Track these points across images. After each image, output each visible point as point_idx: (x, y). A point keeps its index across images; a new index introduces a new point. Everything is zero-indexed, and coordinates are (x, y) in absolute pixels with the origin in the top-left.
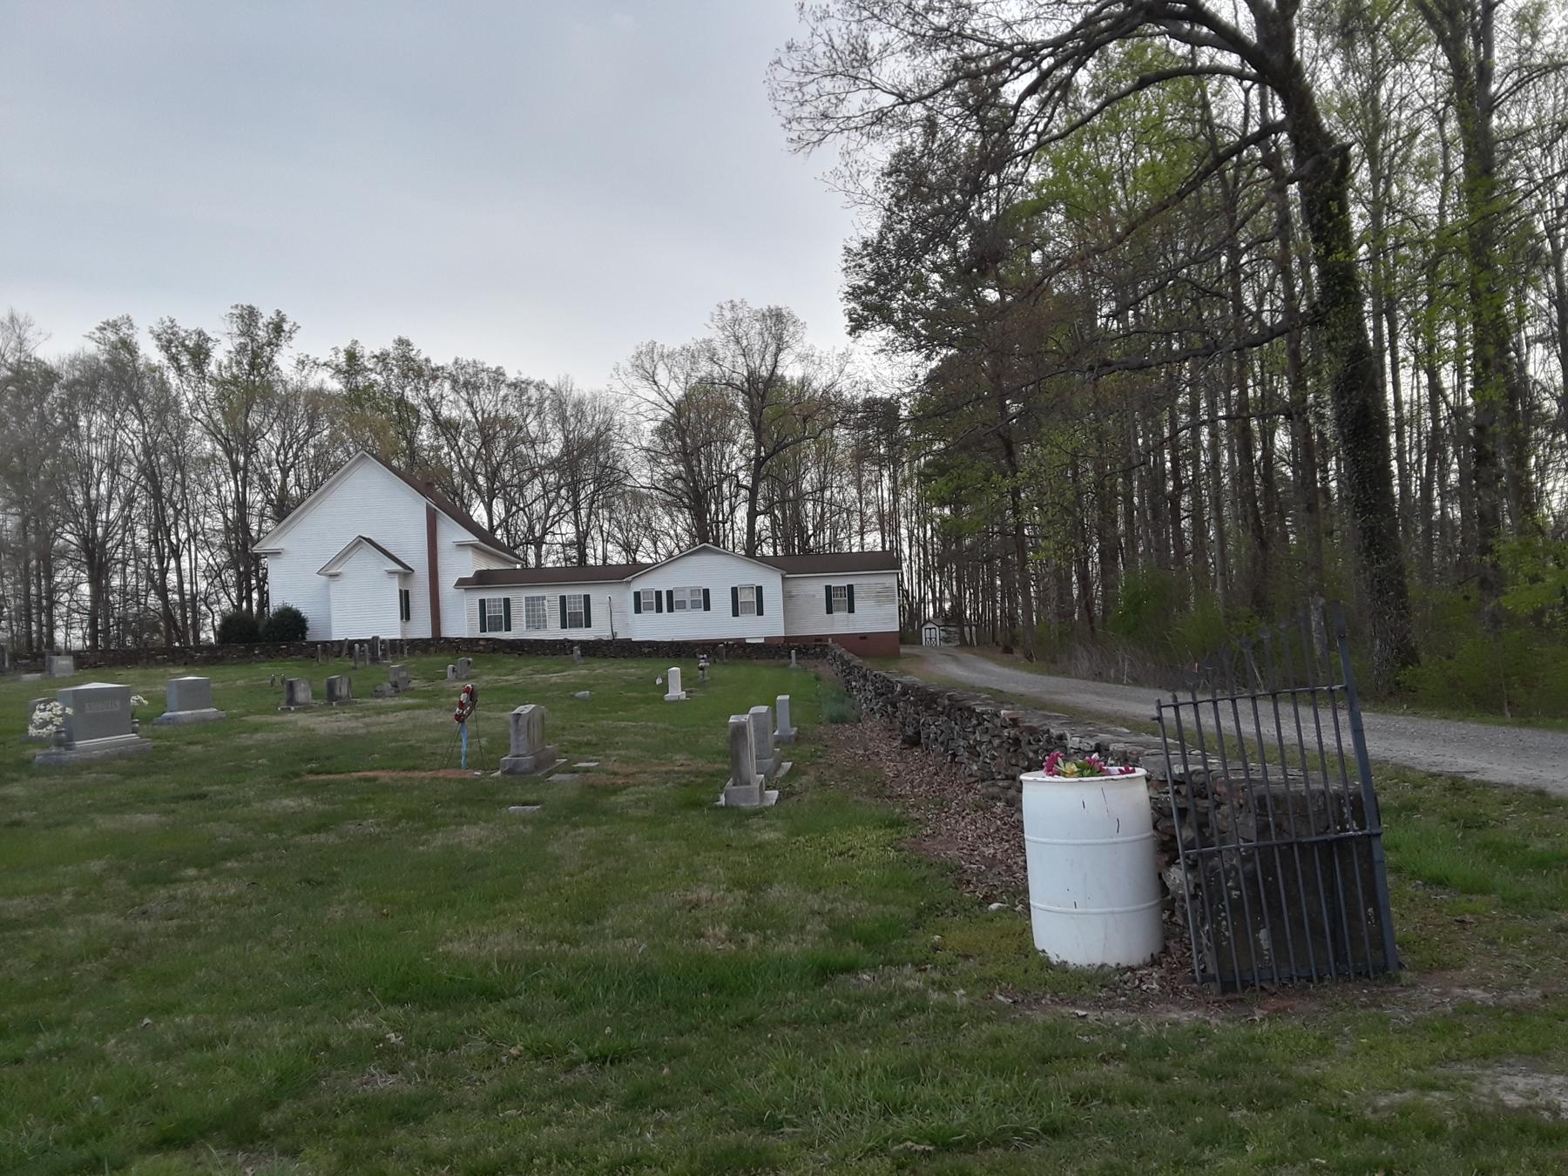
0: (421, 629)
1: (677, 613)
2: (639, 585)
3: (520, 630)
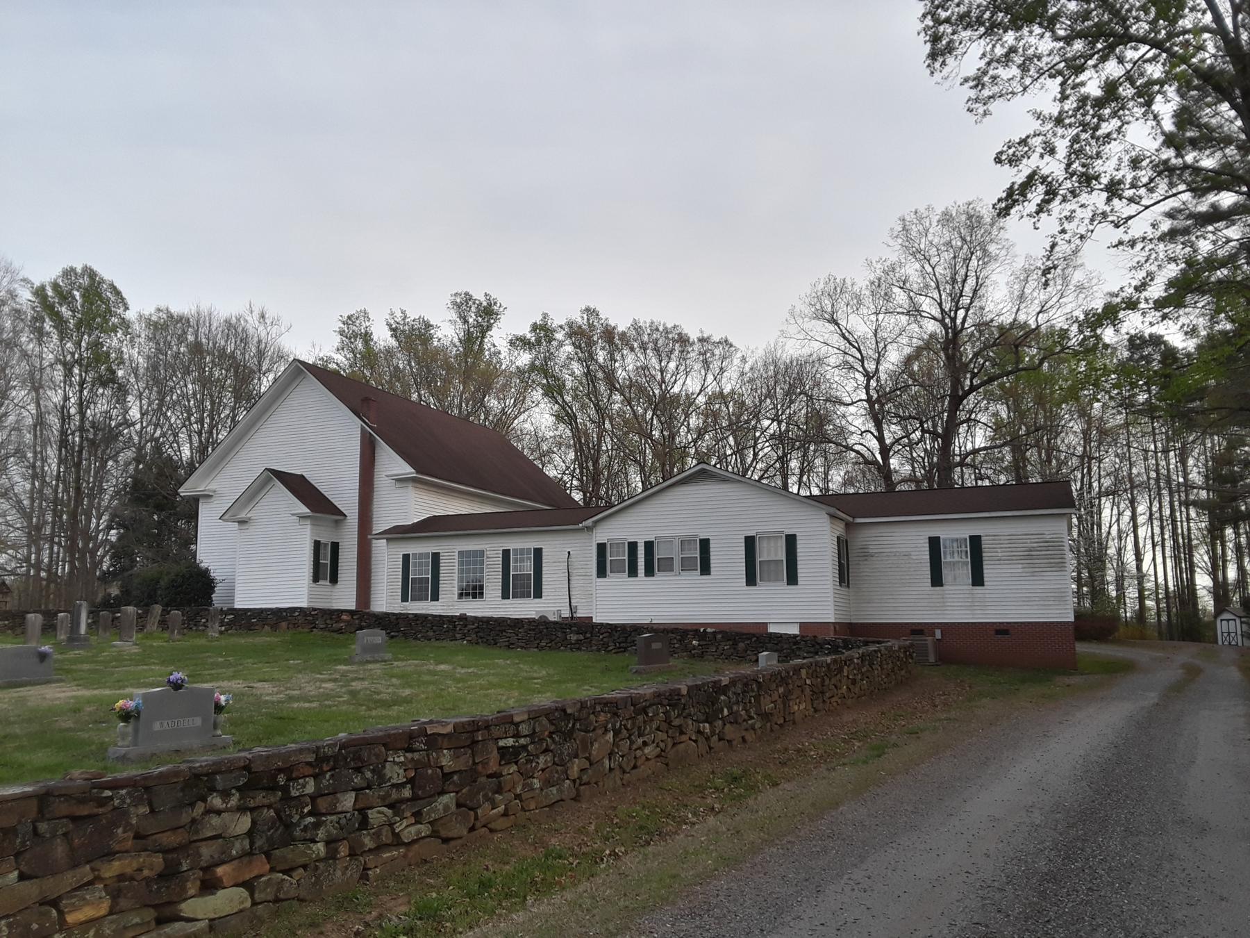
0: (344, 597)
1: (659, 577)
2: (604, 534)
3: (449, 604)
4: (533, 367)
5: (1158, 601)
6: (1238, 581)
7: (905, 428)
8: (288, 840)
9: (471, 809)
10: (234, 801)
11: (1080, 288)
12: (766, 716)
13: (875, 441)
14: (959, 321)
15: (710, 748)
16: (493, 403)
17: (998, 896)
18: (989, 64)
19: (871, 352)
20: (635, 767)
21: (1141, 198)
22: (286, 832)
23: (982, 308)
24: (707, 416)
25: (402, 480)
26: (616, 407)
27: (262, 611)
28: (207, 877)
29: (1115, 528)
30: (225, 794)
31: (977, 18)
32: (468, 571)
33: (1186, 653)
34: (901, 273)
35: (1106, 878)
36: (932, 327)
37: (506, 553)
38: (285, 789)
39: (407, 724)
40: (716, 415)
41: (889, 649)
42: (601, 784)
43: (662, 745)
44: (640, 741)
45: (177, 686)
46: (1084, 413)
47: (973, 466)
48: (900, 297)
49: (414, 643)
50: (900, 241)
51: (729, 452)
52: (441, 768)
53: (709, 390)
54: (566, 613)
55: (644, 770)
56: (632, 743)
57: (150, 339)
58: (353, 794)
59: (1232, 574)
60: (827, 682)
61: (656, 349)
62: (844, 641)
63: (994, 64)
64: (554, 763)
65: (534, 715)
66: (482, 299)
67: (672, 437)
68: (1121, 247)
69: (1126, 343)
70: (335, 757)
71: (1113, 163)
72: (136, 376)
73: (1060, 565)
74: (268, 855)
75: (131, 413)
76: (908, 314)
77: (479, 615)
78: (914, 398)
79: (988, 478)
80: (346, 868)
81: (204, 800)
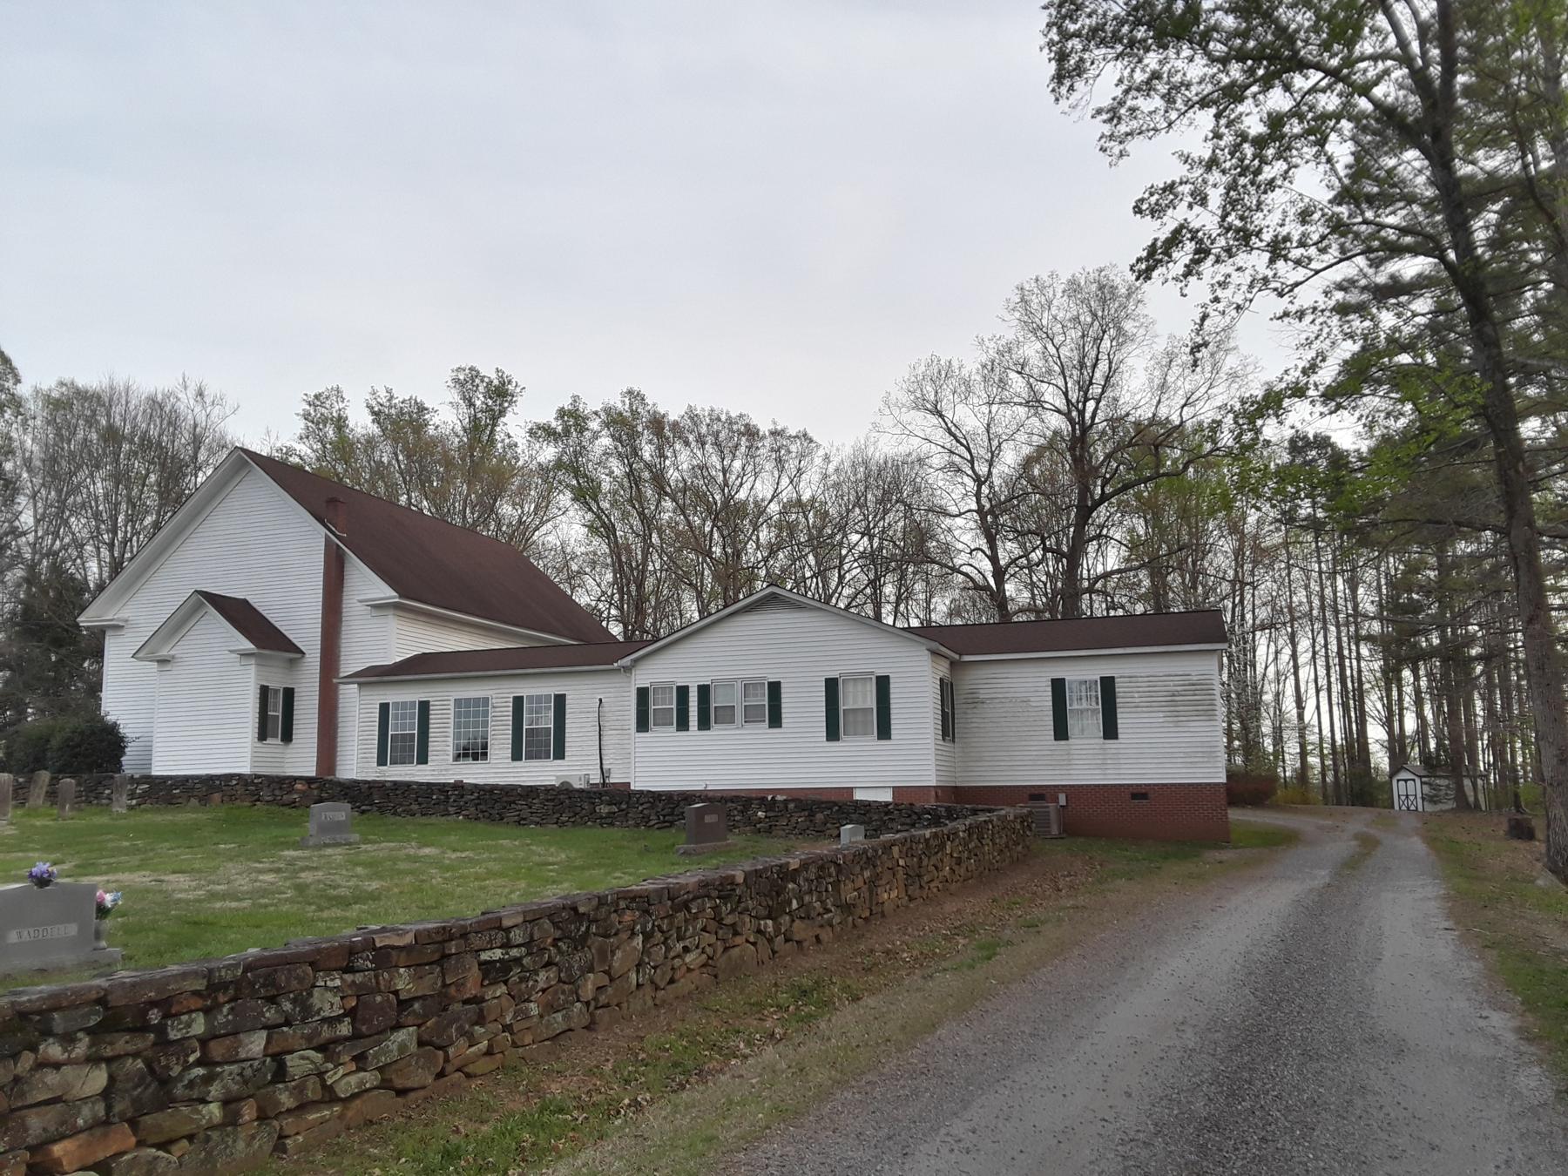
0: (300, 760)
1: (717, 731)
2: (646, 675)
3: (442, 768)
4: (559, 464)
5: (1322, 757)
6: (1417, 732)
7: (1022, 546)
8: (165, 1101)
9: (439, 1048)
10: (81, 1049)
11: (1233, 376)
12: (847, 908)
13: (987, 562)
14: (1088, 415)
15: (774, 952)
16: (506, 509)
17: (1145, 1153)
18: (1127, 92)
19: (982, 452)
20: (672, 981)
21: (1310, 260)
22: (163, 1091)
23: (1116, 400)
24: (781, 530)
25: (379, 607)
26: (666, 516)
27: (187, 778)
28: (38, 1159)
29: (1271, 669)
30: (68, 1039)
31: (1113, 32)
32: (467, 725)
33: (1359, 820)
34: (1019, 354)
35: (1283, 1122)
36: (1056, 422)
37: (518, 701)
38: (161, 1030)
39: (349, 933)
40: (792, 528)
41: (1003, 819)
42: (625, 1005)
43: (709, 950)
44: (679, 946)
45: (42, 881)
46: (1235, 528)
47: (1106, 594)
48: (1017, 384)
49: (393, 819)
50: (1017, 315)
51: (808, 574)
52: (396, 993)
53: (784, 497)
54: (596, 779)
55: (684, 985)
56: (668, 949)
57: (48, 423)
58: (264, 1034)
59: (1410, 724)
60: (925, 862)
61: (717, 444)
62: (948, 809)
63: (1134, 93)
64: (560, 981)
65: (532, 918)
66: (493, 376)
67: (737, 554)
68: (1286, 320)
69: (1286, 444)
70: (237, 983)
71: (1275, 218)
72: (30, 470)
73: (1210, 714)
74: (133, 1123)
75: (23, 518)
76: (1027, 404)
77: (481, 782)
78: (1034, 510)
79: (1123, 607)
80: (253, 1137)
81: (33, 1048)
